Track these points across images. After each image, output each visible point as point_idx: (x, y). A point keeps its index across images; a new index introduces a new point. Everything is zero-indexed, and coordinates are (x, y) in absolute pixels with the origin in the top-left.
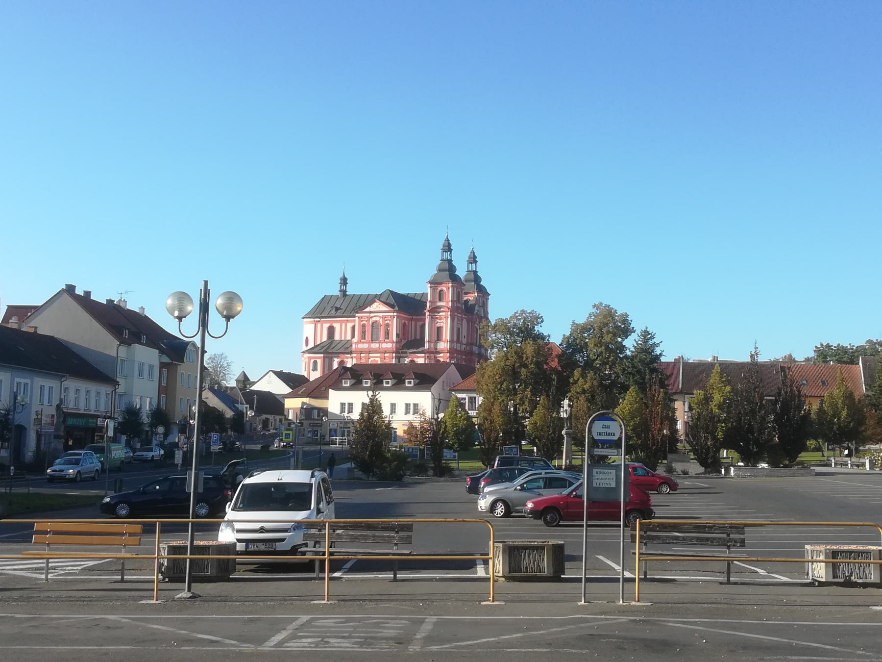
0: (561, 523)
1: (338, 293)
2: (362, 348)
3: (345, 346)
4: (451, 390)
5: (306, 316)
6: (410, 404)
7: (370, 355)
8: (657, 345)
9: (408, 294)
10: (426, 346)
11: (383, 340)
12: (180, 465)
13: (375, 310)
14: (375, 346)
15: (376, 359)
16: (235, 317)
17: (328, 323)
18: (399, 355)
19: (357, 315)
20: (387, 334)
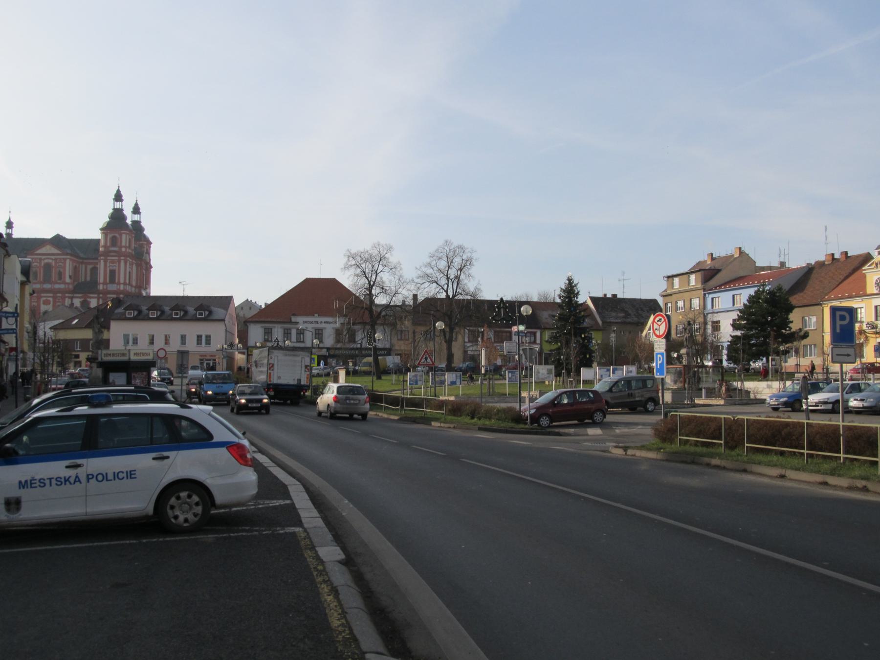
6: (128, 335)
7: (42, 295)
12: (495, 362)
14: (47, 286)
15: (49, 299)
20: (60, 275)
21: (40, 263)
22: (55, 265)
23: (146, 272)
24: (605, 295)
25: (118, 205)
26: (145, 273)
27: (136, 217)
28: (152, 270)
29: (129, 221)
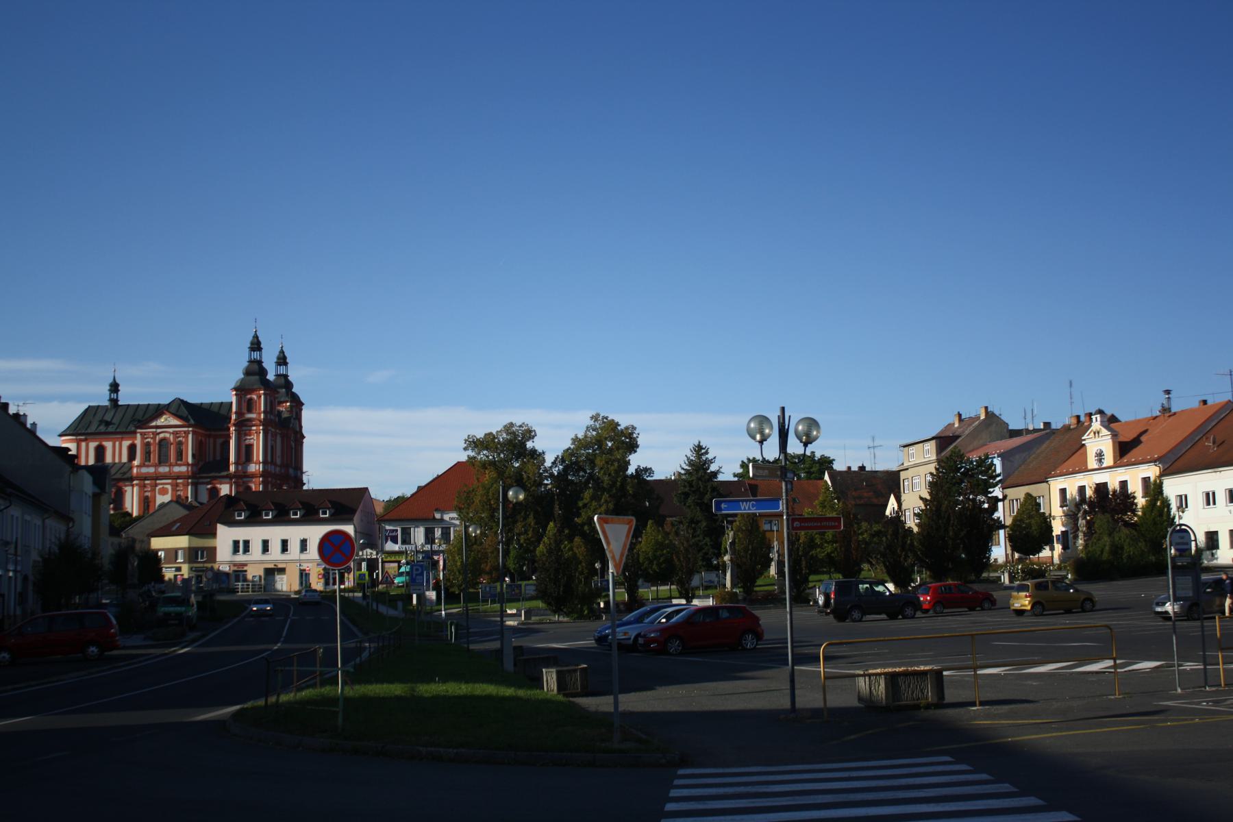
0: (1045, 613)
1: (107, 403)
2: (145, 473)
3: (122, 471)
4: (381, 520)
5: (65, 433)
7: (158, 482)
8: (711, 462)
9: (202, 404)
10: (232, 468)
11: (174, 461)
13: (164, 424)
14: (164, 469)
16: (813, 443)
17: (96, 441)
18: (196, 481)
19: (139, 431)
20: (180, 455)
21: (154, 438)
22: (174, 440)
23: (295, 445)
24: (849, 468)
25: (256, 355)
26: (294, 446)
27: (282, 370)
28: (305, 440)
29: (271, 377)
